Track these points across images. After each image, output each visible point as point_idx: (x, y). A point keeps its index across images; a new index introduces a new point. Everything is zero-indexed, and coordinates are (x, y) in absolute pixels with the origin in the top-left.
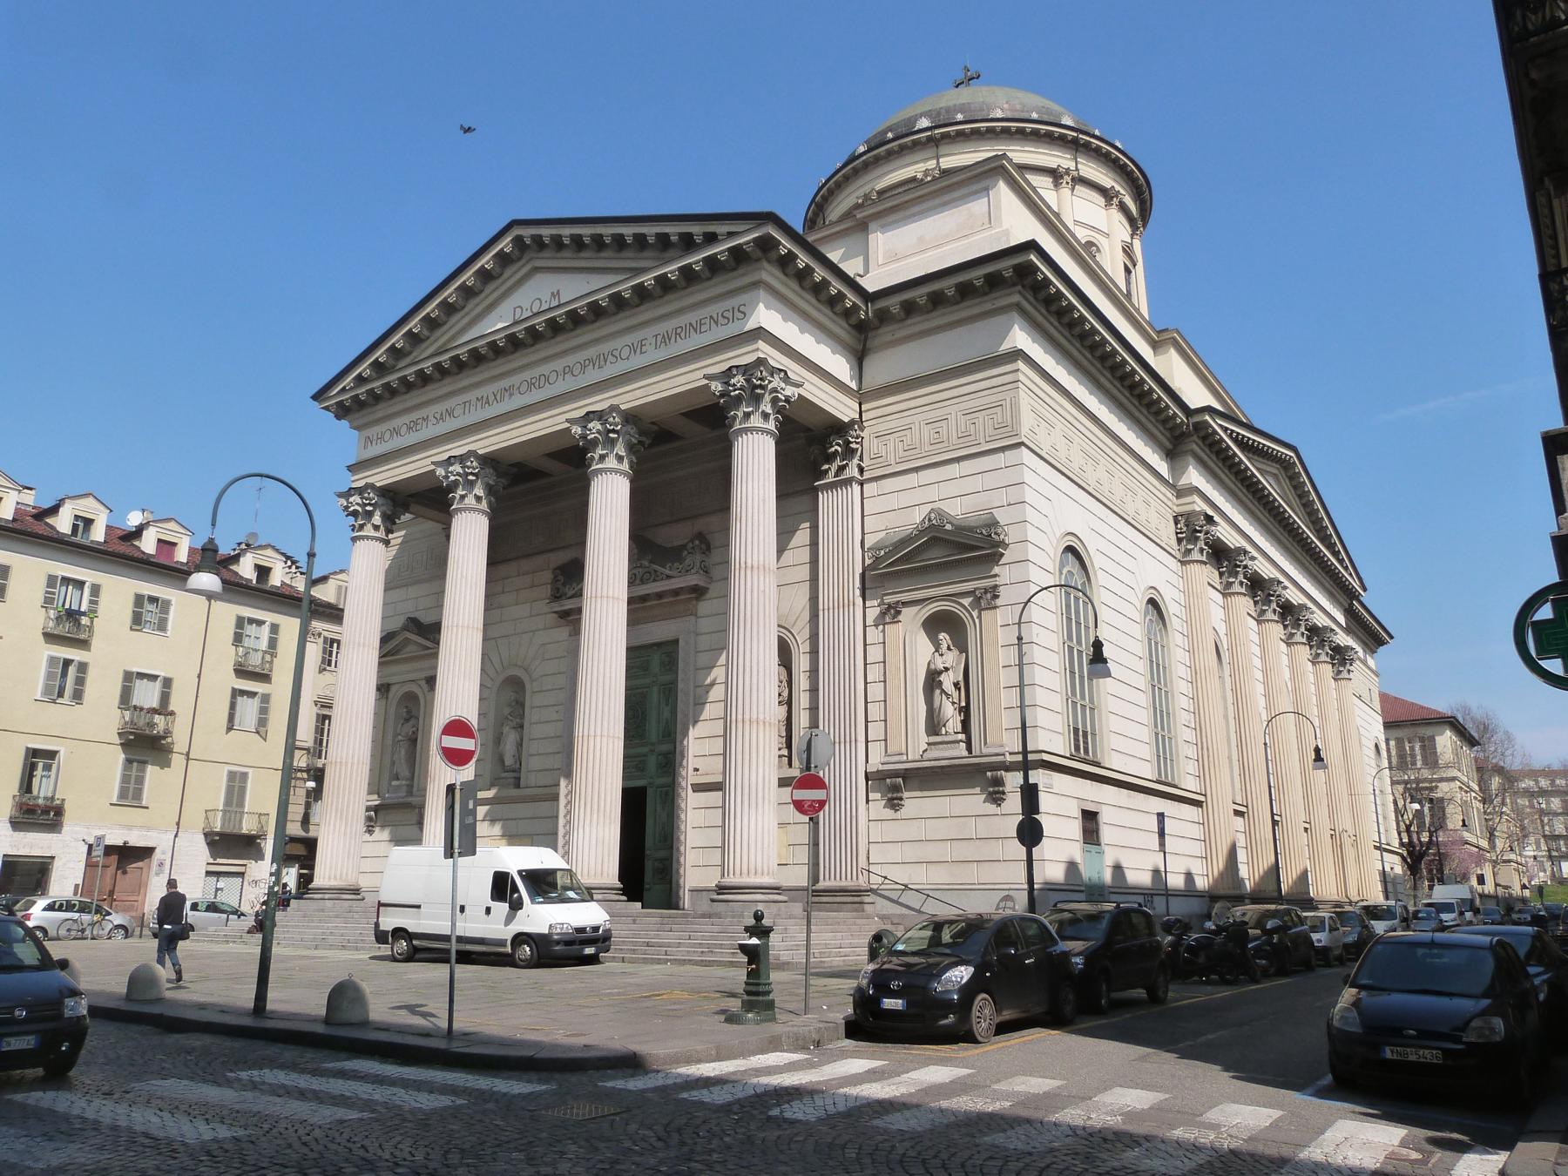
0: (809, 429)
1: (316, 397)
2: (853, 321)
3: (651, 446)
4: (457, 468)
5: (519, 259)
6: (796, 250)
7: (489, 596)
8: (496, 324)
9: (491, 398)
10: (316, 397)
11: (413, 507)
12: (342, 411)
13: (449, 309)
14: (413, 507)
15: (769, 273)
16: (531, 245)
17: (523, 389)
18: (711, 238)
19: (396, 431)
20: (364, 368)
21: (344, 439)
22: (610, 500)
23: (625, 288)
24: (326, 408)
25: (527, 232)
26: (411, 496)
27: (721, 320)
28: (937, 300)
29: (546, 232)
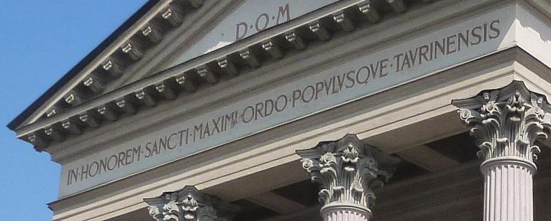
3: (392, 181)
9: (212, 127)
12: (43, 142)
17: (247, 117)
20: (67, 93)
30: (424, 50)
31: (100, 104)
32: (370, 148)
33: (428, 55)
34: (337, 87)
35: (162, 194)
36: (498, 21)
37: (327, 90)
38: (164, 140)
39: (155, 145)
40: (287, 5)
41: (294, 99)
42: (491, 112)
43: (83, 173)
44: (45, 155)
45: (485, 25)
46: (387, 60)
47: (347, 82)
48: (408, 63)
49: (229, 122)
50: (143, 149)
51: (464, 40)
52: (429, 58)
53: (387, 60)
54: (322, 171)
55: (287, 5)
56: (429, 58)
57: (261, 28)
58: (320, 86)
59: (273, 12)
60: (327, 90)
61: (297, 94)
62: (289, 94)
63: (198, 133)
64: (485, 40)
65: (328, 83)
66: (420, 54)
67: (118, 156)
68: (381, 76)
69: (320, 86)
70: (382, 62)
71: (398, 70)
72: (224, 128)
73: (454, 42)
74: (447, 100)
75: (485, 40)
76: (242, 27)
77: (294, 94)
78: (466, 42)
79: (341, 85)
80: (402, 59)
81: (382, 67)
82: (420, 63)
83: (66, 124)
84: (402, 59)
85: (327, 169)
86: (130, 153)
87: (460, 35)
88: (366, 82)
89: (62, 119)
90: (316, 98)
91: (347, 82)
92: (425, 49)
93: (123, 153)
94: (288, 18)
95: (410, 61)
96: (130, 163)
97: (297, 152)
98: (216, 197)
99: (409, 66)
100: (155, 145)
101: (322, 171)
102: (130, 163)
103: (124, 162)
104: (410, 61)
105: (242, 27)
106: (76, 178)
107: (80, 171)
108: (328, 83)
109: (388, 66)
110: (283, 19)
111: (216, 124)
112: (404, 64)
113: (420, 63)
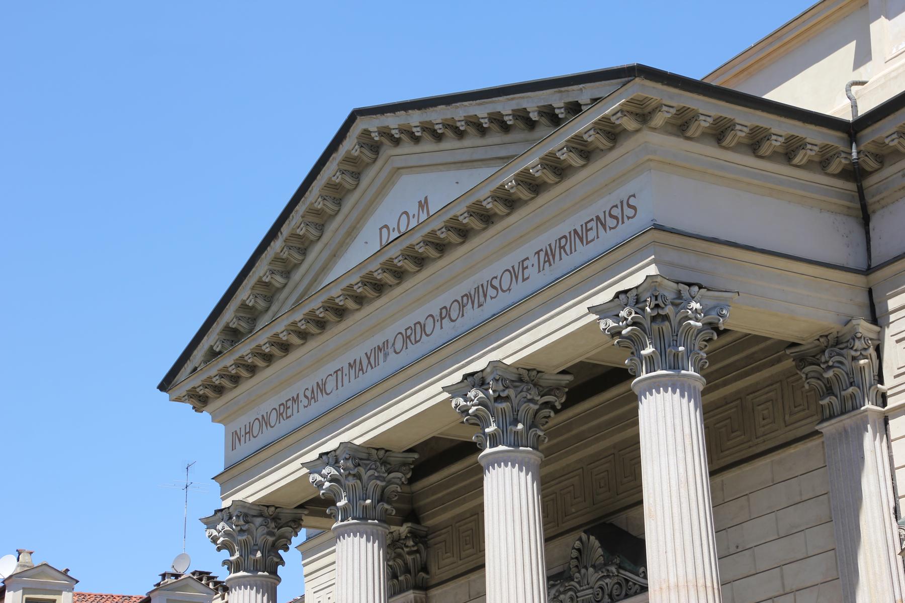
0: (794, 345)
1: (163, 387)
2: (835, 167)
3: (565, 406)
4: (329, 470)
5: (375, 160)
6: (306, 309)
7: (721, 529)
8: (362, 251)
9: (365, 362)
10: (163, 387)
11: (307, 520)
12: (200, 401)
13: (303, 246)
14: (307, 520)
15: (655, 141)
16: (366, 143)
17: (399, 345)
18: (575, 109)
19: (265, 421)
20: (211, 340)
21: (203, 438)
22: (509, 502)
23: (508, 179)
24: (178, 399)
25: (372, 124)
26: (301, 506)
27: (611, 222)
28: (337, 194)
29: (392, 121)
30: (563, 241)
31: (261, 339)
32: (525, 371)
33: (567, 248)
34: (482, 299)
35: (317, 456)
36: (634, 196)
37: (473, 303)
38: (320, 383)
39: (313, 391)
40: (426, 198)
41: (442, 319)
42: (630, 318)
43: (246, 434)
44: (205, 416)
45: (622, 202)
46: (527, 258)
47: (491, 292)
48: (549, 261)
49: (381, 355)
50: (302, 397)
51: (602, 224)
52: (568, 252)
53: (527, 258)
54: (470, 411)
55: (426, 198)
56: (568, 252)
57: (403, 230)
58: (465, 299)
59: (413, 209)
60: (473, 303)
61: (444, 311)
62: (436, 313)
63: (352, 372)
64: (623, 222)
65: (473, 293)
66: (560, 248)
67: (460, 300)
68: (524, 280)
69: (465, 299)
70: (586, 223)
71: (539, 271)
72: (377, 363)
73: (591, 229)
74: (583, 308)
75: (623, 222)
76: (385, 231)
77: (441, 314)
78: (604, 226)
79: (485, 296)
80: (542, 254)
81: (587, 231)
82: (561, 259)
83: (535, 170)
84: (542, 254)
85: (474, 408)
86: (290, 403)
87: (598, 218)
88: (509, 289)
89: (530, 163)
90: (463, 315)
91: (491, 292)
92: (564, 240)
93: (283, 404)
94: (428, 213)
95: (551, 257)
96: (593, 240)
97: (445, 389)
98: (534, 369)
99: (550, 265)
100: (313, 391)
101: (624, 332)
102: (593, 240)
103: (284, 415)
104: (551, 257)
105: (385, 231)
106: (240, 440)
107: (243, 433)
108: (473, 293)
109: (530, 266)
110: (423, 217)
111: (369, 359)
112: (545, 262)
113: (561, 259)
